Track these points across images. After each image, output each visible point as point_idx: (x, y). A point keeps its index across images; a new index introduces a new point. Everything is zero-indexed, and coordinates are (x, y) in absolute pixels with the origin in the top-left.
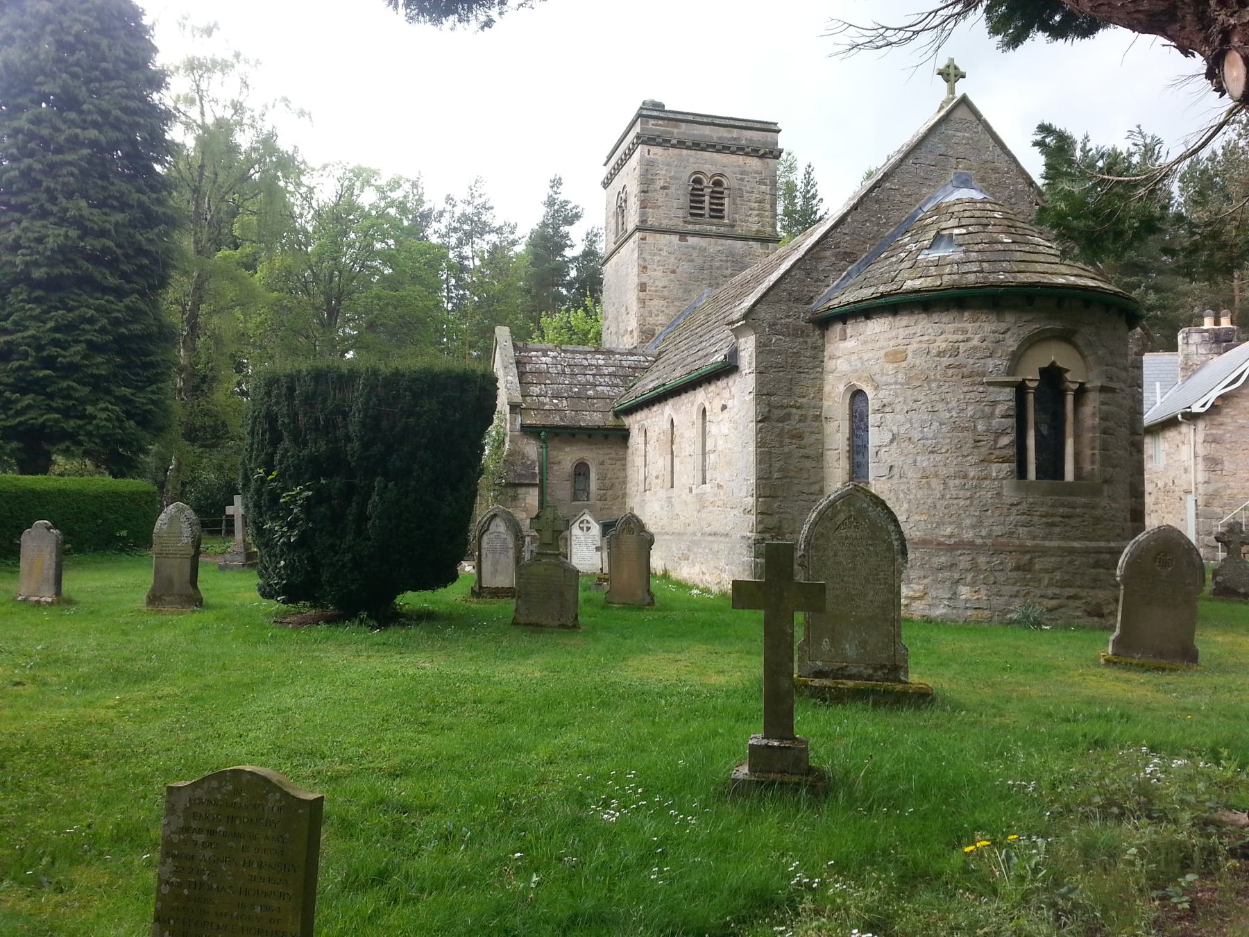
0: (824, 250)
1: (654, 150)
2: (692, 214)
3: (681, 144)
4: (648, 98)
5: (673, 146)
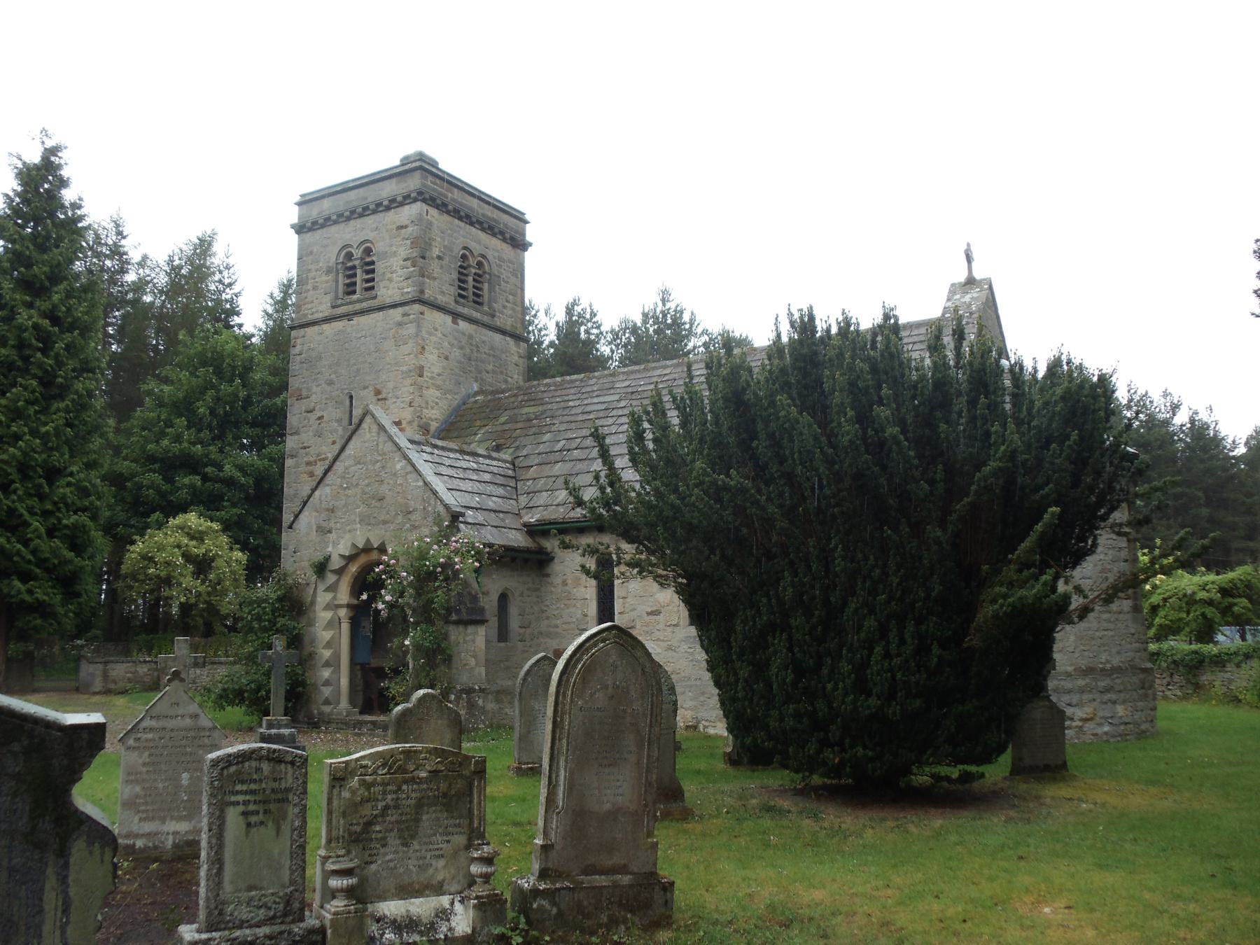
1: (433, 212)
2: (460, 295)
4: (431, 152)
5: (448, 212)
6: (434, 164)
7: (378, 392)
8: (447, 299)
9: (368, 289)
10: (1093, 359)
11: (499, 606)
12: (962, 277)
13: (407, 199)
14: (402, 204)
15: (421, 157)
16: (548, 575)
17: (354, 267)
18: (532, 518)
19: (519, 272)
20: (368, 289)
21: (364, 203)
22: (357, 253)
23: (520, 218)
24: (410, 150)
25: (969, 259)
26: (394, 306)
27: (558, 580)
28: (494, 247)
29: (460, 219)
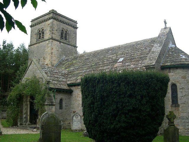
0: (181, 54)
1: (55, 21)
2: (61, 38)
3: (61, 21)
4: (55, 9)
5: (59, 21)
6: (56, 11)
7: (44, 58)
8: (58, 38)
9: (43, 37)
11: (60, 102)
12: (164, 27)
13: (50, 19)
14: (49, 20)
15: (53, 10)
16: (72, 95)
17: (40, 33)
18: (69, 83)
19: (76, 33)
20: (43, 37)
22: (41, 30)
24: (51, 9)
25: (165, 23)
26: (47, 40)
27: (74, 96)
28: (70, 28)
29: (61, 22)
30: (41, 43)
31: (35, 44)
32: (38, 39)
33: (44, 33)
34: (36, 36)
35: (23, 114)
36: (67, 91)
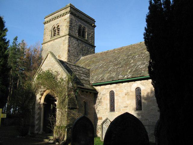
6: (74, 7)
9: (58, 34)
10: (145, 20)
14: (66, 14)
17: (55, 30)
21: (58, 16)
22: (56, 26)
23: (94, 21)
26: (63, 36)
30: (55, 40)
31: (49, 41)
32: (52, 36)
33: (60, 29)
34: (51, 32)
35: (35, 120)
36: (91, 91)
